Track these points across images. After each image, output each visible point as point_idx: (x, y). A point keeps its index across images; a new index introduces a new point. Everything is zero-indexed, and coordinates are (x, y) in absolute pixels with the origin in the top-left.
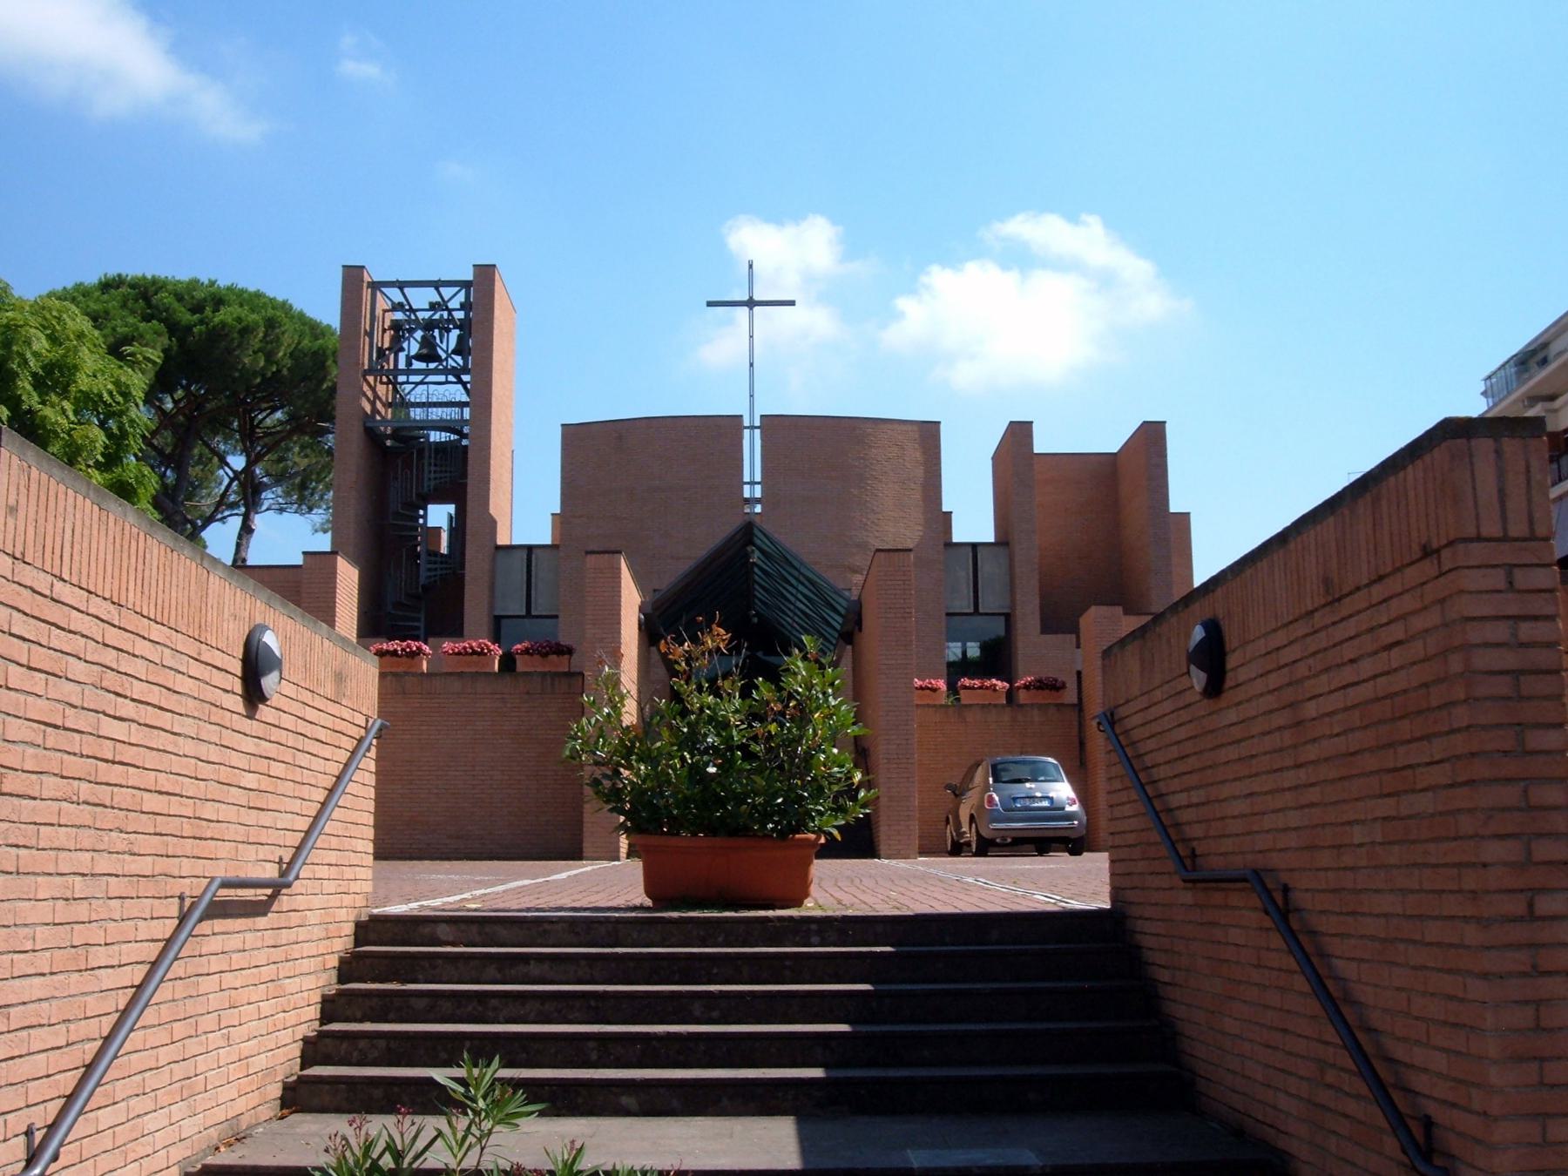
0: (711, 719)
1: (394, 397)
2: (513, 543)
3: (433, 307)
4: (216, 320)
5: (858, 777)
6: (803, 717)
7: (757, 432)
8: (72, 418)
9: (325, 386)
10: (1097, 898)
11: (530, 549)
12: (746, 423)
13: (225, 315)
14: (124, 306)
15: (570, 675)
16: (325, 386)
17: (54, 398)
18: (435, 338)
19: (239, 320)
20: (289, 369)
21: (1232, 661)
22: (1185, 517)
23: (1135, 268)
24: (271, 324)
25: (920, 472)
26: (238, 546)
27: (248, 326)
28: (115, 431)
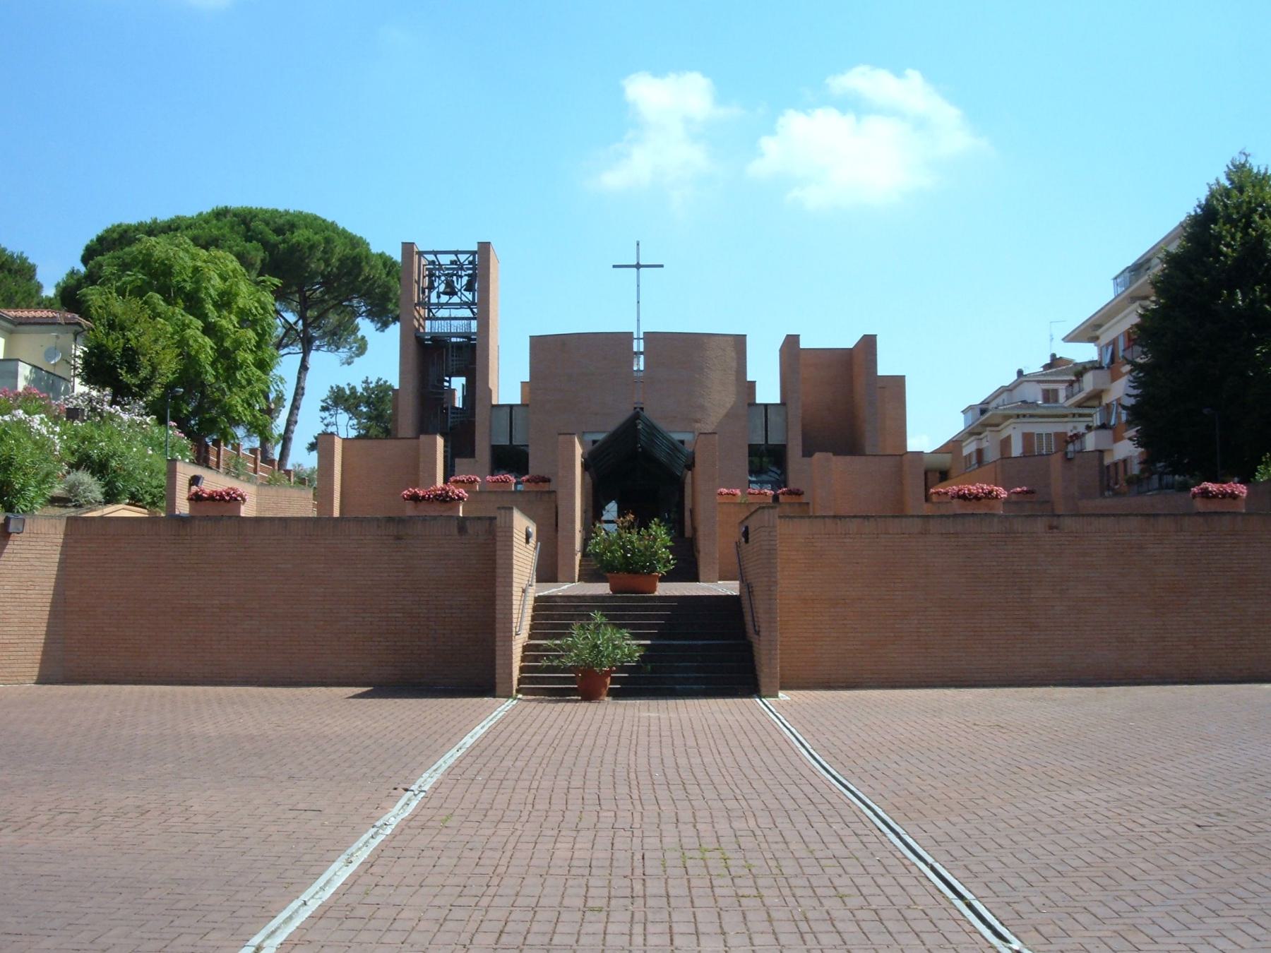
0: (629, 541)
1: (429, 314)
2: (500, 403)
3: (452, 263)
4: (294, 240)
5: (671, 557)
6: (655, 539)
7: (642, 341)
8: (237, 325)
9: (360, 279)
10: (736, 593)
11: (511, 407)
12: (635, 336)
13: (299, 236)
14: (232, 228)
15: (550, 492)
16: (360, 279)
17: (225, 313)
18: (453, 282)
19: (308, 240)
20: (337, 268)
21: (750, 536)
22: (898, 383)
23: (947, 115)
24: (328, 241)
25: (734, 364)
26: (299, 379)
27: (314, 244)
28: (260, 331)
